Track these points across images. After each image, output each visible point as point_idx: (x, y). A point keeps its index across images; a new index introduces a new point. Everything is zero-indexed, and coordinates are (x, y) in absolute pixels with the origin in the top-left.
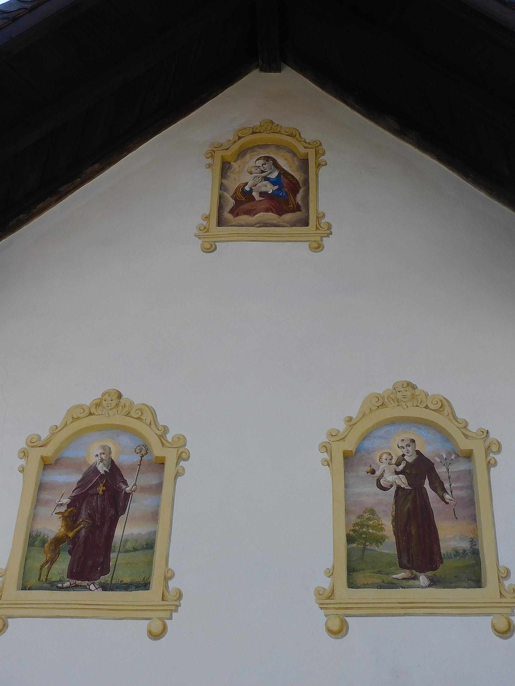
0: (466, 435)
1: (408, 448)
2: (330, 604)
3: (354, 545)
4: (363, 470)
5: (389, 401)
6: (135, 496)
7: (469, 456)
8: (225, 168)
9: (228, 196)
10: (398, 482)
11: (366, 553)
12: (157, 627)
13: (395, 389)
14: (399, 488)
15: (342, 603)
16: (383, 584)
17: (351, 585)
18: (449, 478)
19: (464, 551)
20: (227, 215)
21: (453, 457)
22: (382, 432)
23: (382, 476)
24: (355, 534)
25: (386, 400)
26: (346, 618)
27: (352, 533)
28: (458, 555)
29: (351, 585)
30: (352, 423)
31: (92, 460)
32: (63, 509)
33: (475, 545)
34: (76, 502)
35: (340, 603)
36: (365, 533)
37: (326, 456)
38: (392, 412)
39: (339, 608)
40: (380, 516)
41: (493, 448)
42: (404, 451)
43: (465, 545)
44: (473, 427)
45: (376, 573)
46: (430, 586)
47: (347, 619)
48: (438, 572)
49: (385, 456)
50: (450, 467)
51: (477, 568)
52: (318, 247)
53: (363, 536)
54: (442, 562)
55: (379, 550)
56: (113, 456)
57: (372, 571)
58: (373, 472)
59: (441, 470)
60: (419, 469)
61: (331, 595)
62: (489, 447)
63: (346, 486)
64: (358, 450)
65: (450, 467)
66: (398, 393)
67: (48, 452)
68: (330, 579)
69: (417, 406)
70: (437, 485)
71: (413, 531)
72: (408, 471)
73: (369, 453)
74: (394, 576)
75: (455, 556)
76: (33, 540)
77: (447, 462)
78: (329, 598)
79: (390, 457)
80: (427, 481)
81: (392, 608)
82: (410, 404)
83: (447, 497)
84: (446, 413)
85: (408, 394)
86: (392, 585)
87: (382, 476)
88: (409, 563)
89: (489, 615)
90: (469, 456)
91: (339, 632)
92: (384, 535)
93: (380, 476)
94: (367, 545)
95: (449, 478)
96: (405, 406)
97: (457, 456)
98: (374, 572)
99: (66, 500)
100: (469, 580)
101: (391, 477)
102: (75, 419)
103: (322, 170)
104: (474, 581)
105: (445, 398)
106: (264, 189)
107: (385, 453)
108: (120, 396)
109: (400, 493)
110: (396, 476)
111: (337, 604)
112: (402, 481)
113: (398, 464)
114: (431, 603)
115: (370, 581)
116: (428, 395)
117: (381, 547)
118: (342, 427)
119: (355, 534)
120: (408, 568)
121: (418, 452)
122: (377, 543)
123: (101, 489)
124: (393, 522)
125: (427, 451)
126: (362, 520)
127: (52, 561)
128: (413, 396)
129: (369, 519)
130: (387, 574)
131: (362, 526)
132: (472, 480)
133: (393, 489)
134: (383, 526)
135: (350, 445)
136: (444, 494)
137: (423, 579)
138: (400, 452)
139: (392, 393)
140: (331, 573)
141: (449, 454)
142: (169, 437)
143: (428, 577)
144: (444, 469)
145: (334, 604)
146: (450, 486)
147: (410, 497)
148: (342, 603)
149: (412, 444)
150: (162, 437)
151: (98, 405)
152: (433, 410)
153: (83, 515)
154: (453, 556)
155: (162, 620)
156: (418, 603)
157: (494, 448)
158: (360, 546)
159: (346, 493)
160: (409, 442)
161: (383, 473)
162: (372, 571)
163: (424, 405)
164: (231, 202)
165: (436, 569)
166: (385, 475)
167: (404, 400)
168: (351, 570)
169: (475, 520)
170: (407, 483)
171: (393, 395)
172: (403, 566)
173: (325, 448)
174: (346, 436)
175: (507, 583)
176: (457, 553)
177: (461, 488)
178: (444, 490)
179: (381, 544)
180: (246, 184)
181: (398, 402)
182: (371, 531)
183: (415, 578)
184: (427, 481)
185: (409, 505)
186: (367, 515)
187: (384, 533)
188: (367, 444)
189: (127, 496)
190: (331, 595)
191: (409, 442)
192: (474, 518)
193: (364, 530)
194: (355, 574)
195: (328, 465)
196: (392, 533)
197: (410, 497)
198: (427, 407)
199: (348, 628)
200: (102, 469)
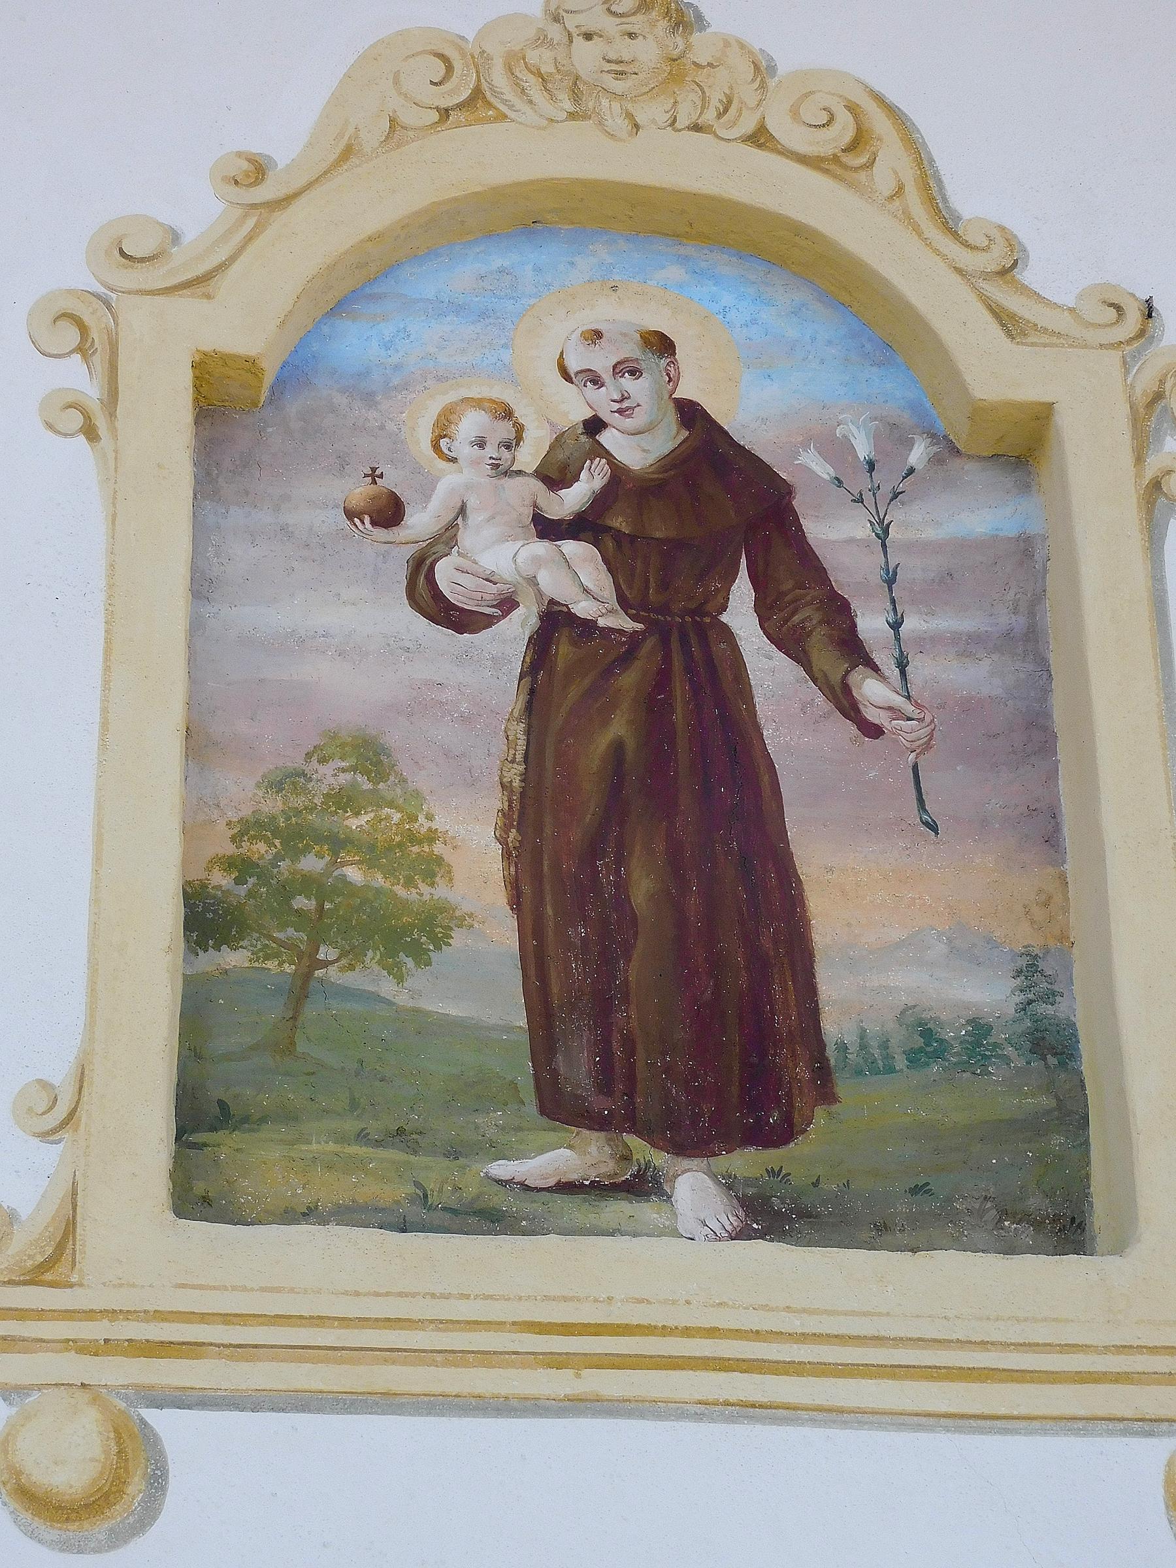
0: (1013, 316)
1: (627, 382)
2: (40, 1315)
3: (234, 958)
4: (321, 499)
5: (516, 83)
7: (1020, 448)
10: (554, 584)
11: (310, 1011)
13: (557, 19)
14: (555, 620)
15: (127, 1315)
16: (416, 1213)
17: (197, 1195)
18: (890, 581)
19: (979, 1029)
21: (918, 454)
22: (460, 275)
23: (447, 537)
24: (242, 890)
25: (499, 78)
26: (151, 1415)
27: (221, 879)
28: (938, 1055)
29: (197, 1195)
30: (266, 192)
33: (1050, 997)
35: (112, 1314)
36: (308, 884)
37: (78, 377)
38: (531, 149)
39: (107, 1348)
40: (420, 781)
42: (602, 401)
43: (989, 994)
44: (1057, 275)
45: (378, 1144)
46: (741, 1234)
47: (159, 1420)
48: (801, 1158)
49: (470, 424)
50: (897, 515)
51: (1057, 1140)
53: (301, 902)
54: (826, 1094)
55: (403, 999)
57: (351, 1125)
58: (389, 512)
59: (835, 532)
60: (700, 517)
62: (1158, 396)
63: (202, 586)
64: (296, 373)
65: (897, 515)
66: (579, 41)
68: (49, 1155)
69: (696, 128)
70: (808, 615)
71: (643, 888)
72: (619, 522)
73: (369, 398)
74: (502, 1169)
75: (915, 1058)
77: (877, 486)
78: (35, 1276)
79: (505, 430)
80: (742, 592)
81: (486, 1358)
82: (652, 112)
83: (873, 692)
84: (883, 178)
85: (647, 51)
86: (486, 1217)
87: (447, 537)
88: (605, 1087)
89: (1150, 1425)
90: (1020, 448)
92: (444, 908)
93: (436, 540)
94: (326, 964)
95: (890, 581)
96: (620, 124)
97: (948, 450)
98: (362, 1137)
100: (1004, 1213)
101: (511, 547)
104: (1038, 1225)
105: (879, 99)
107: (478, 403)
109: (563, 650)
110: (542, 548)
111: (90, 1315)
112: (580, 578)
113: (556, 476)
114: (757, 1335)
115: (333, 1189)
116: (772, 69)
117: (418, 978)
118: (197, 211)
119: (242, 890)
120: (600, 1123)
121: (690, 414)
122: (391, 953)
124: (506, 828)
125: (752, 413)
126: (299, 802)
128: (676, 71)
129: (344, 800)
130: (453, 1153)
131: (294, 837)
132: (1038, 598)
133: (517, 629)
134: (438, 848)
135: (247, 323)
136: (855, 677)
137: (695, 1189)
138: (574, 407)
139: (542, 40)
140: (61, 1115)
141: (895, 436)
143: (729, 1184)
144: (859, 527)
145: (68, 1315)
146: (896, 626)
147: (629, 679)
148: (127, 1315)
149: (654, 365)
152: (803, 159)
154: (901, 1062)
156: (666, 1331)
158: (271, 965)
159: (196, 626)
160: (631, 350)
161: (452, 526)
162: (351, 1125)
163: (748, 125)
165: (784, 1134)
166: (466, 539)
167: (619, 86)
168: (201, 1116)
169: (1051, 840)
170: (608, 592)
171: (547, 54)
172: (559, 1107)
173: (79, 327)
174: (222, 267)
176: (926, 1042)
177: (968, 646)
178: (854, 650)
179: (421, 957)
181: (576, 96)
182: (354, 874)
183: (642, 1186)
184: (742, 592)
185: (620, 727)
186: (330, 776)
187: (441, 891)
188: (357, 344)
190: (55, 1261)
191: (631, 350)
192: (1043, 831)
193: (312, 863)
194: (227, 1143)
195: (90, 432)
196: (499, 897)
197: (629, 679)
198: (760, 138)
199: (158, 1481)
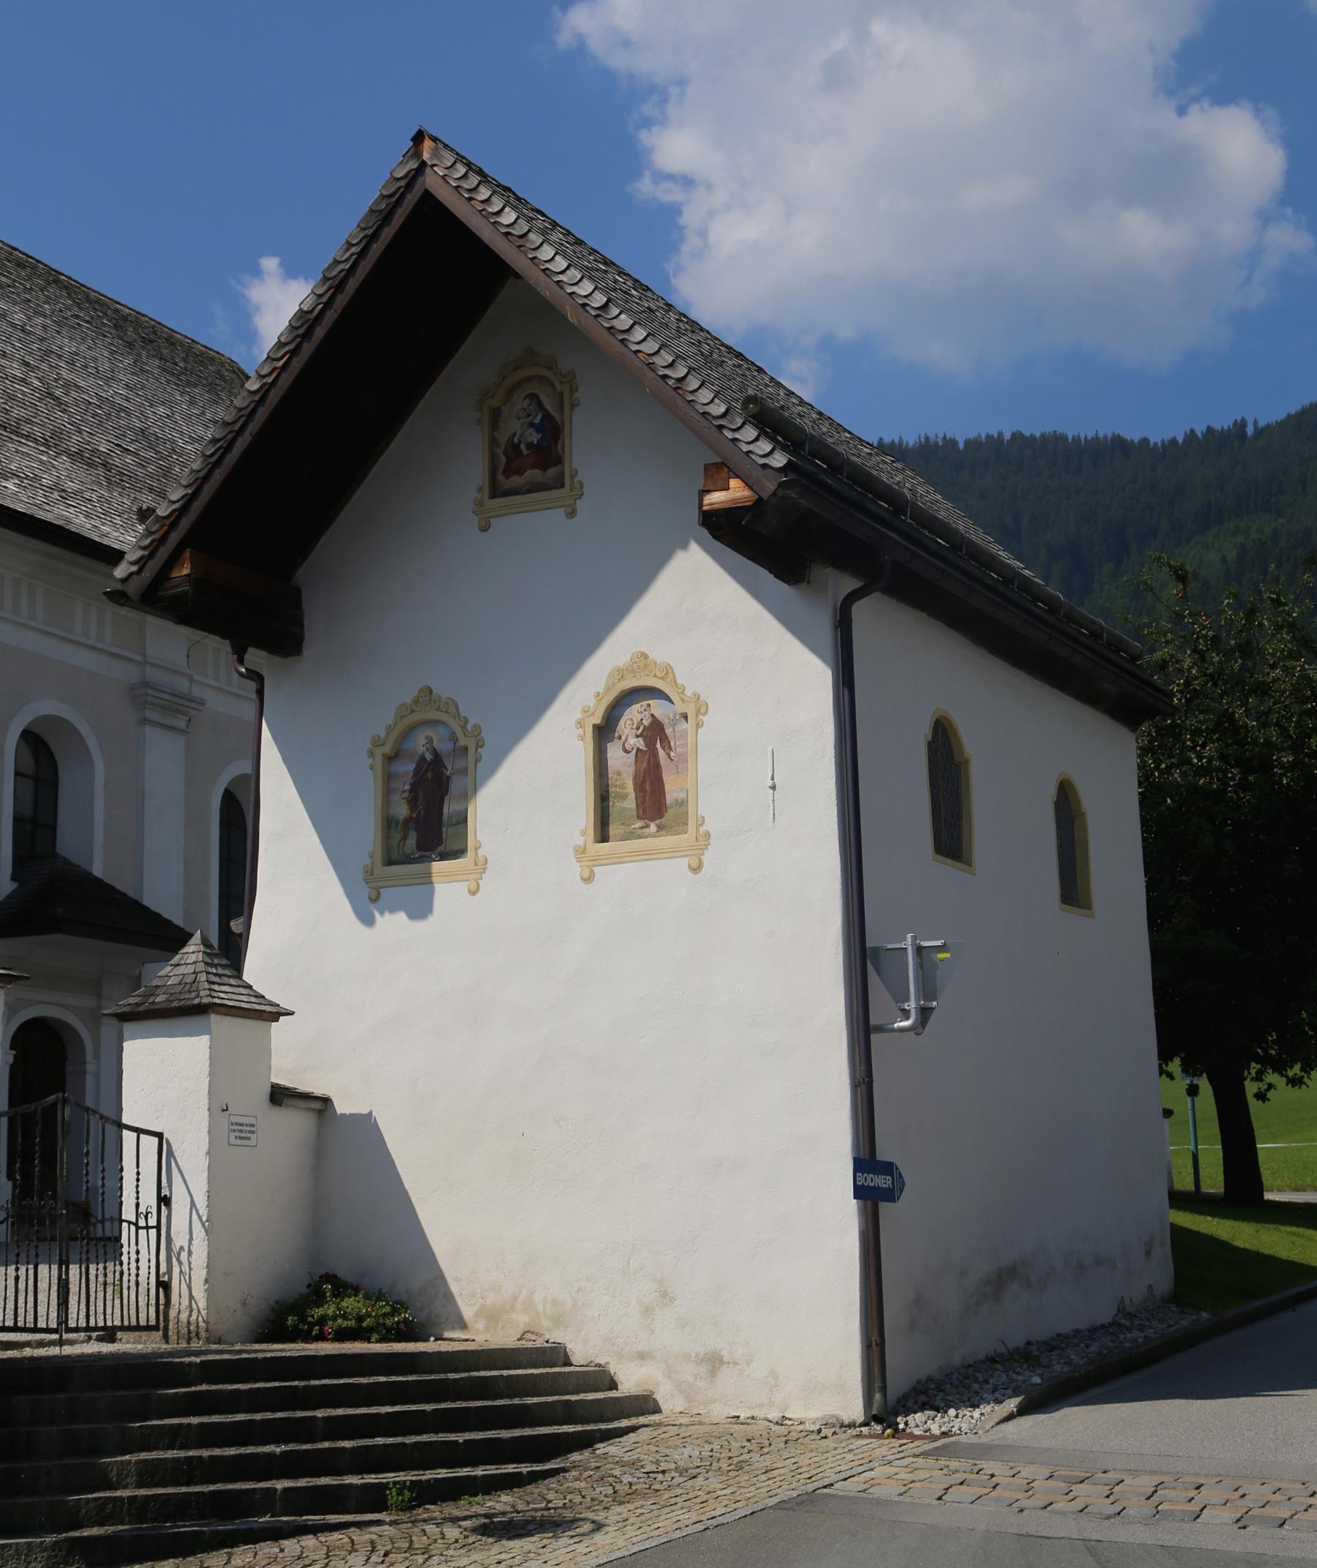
6: (454, 779)
8: (496, 417)
9: (500, 452)
12: (473, 888)
14: (638, 749)
20: (501, 477)
31: (421, 750)
32: (406, 795)
34: (415, 787)
41: (702, 708)
52: (572, 513)
56: (435, 744)
59: (668, 731)
61: (584, 851)
67: (387, 749)
71: (648, 787)
76: (389, 823)
91: (588, 879)
99: (407, 787)
102: (402, 717)
103: (576, 412)
106: (530, 439)
108: (431, 692)
112: (640, 743)
123: (430, 774)
127: (405, 838)
140: (584, 833)
142: (469, 727)
150: (464, 728)
151: (416, 702)
153: (421, 797)
155: (476, 880)
157: (703, 710)
164: (503, 460)
172: (639, 818)
175: (701, 829)
178: (670, 748)
180: (515, 434)
183: (648, 826)
189: (448, 778)
200: (429, 757)
